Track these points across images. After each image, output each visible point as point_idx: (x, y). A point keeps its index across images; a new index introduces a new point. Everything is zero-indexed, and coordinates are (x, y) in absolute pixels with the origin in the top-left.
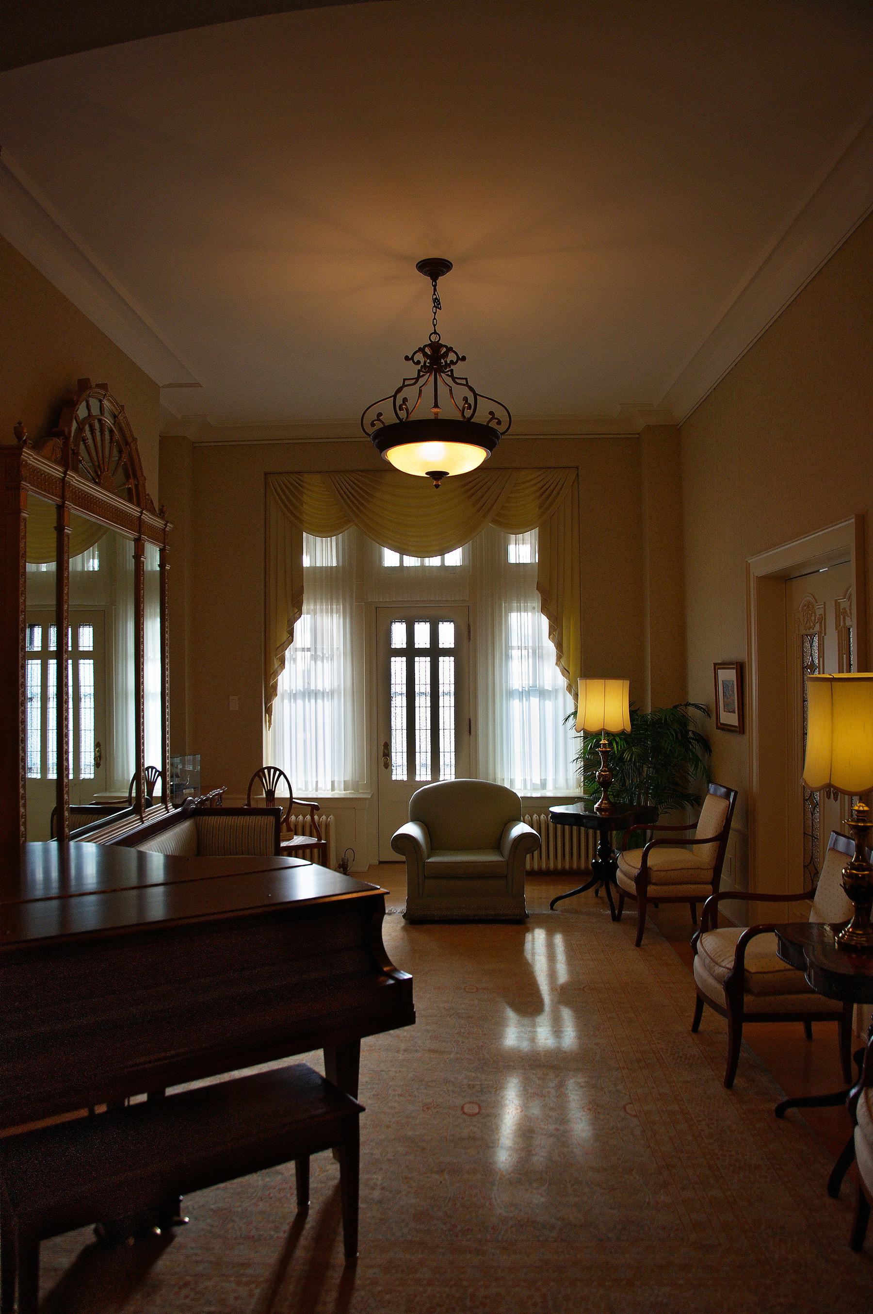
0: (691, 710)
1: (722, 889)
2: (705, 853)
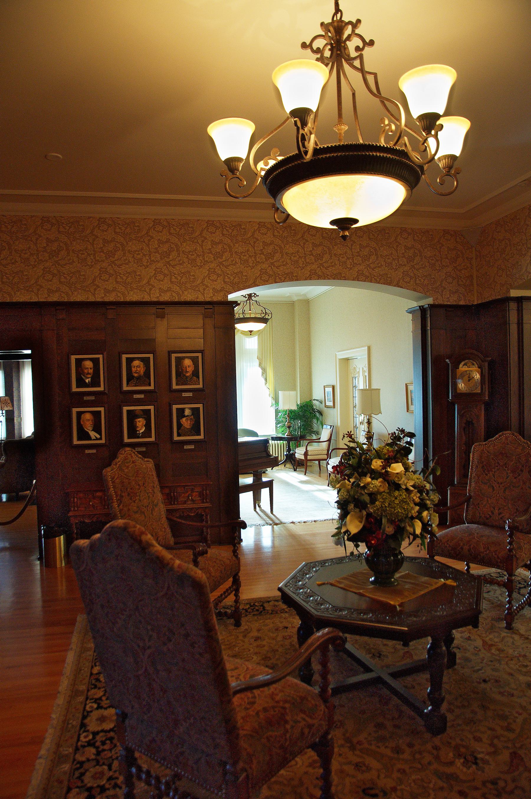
0: (314, 402)
1: (357, 31)
2: (325, 445)
